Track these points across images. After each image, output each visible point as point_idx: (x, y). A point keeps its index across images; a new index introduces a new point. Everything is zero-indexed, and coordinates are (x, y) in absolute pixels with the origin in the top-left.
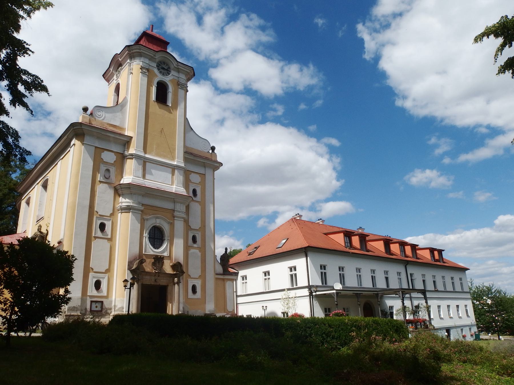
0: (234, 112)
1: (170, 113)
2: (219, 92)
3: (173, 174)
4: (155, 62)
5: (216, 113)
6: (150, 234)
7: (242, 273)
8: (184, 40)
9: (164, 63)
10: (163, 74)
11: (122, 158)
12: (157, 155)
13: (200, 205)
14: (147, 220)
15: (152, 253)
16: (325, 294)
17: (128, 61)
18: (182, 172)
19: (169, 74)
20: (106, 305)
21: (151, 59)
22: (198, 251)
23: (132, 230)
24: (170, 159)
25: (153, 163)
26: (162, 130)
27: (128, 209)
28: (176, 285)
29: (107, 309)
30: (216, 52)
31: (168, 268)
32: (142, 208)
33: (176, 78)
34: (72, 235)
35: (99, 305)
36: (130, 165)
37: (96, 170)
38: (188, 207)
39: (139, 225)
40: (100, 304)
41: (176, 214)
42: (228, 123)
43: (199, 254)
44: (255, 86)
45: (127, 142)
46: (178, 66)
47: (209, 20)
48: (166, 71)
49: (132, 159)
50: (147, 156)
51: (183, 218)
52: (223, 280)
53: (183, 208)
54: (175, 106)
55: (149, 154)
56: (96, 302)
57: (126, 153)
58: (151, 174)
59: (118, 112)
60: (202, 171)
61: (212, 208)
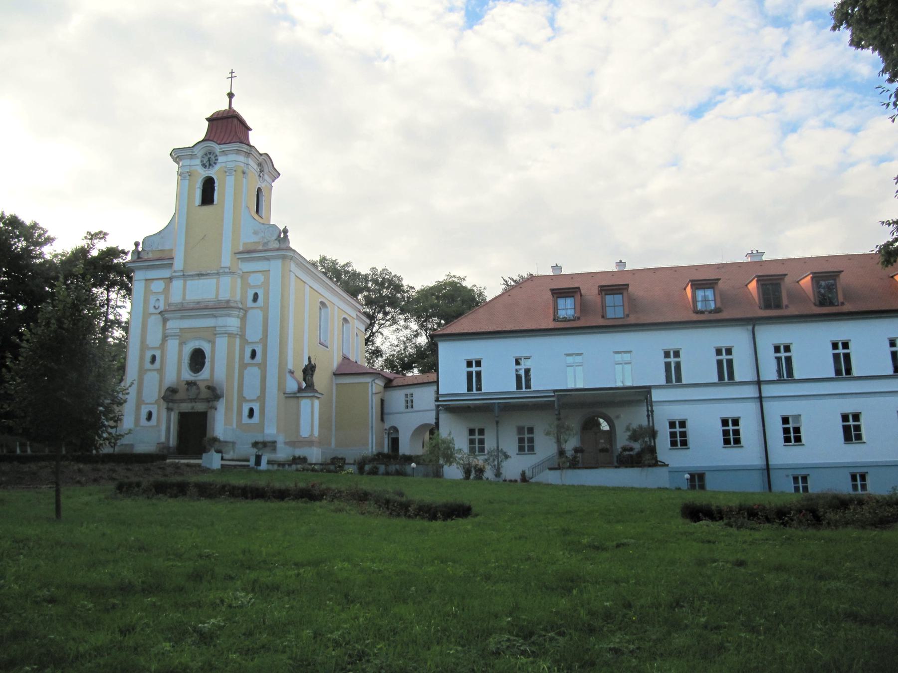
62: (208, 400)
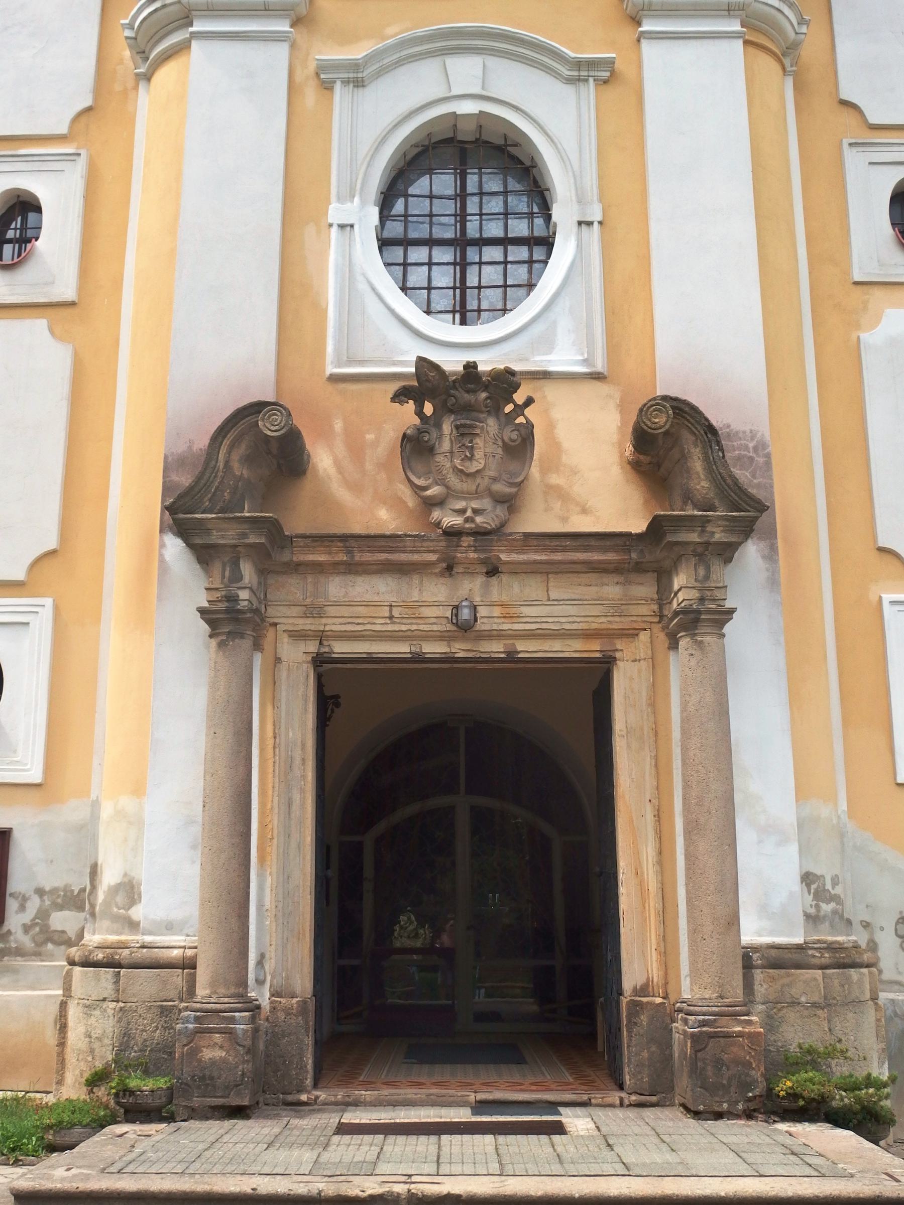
31: (587, 477)
62: (644, 555)
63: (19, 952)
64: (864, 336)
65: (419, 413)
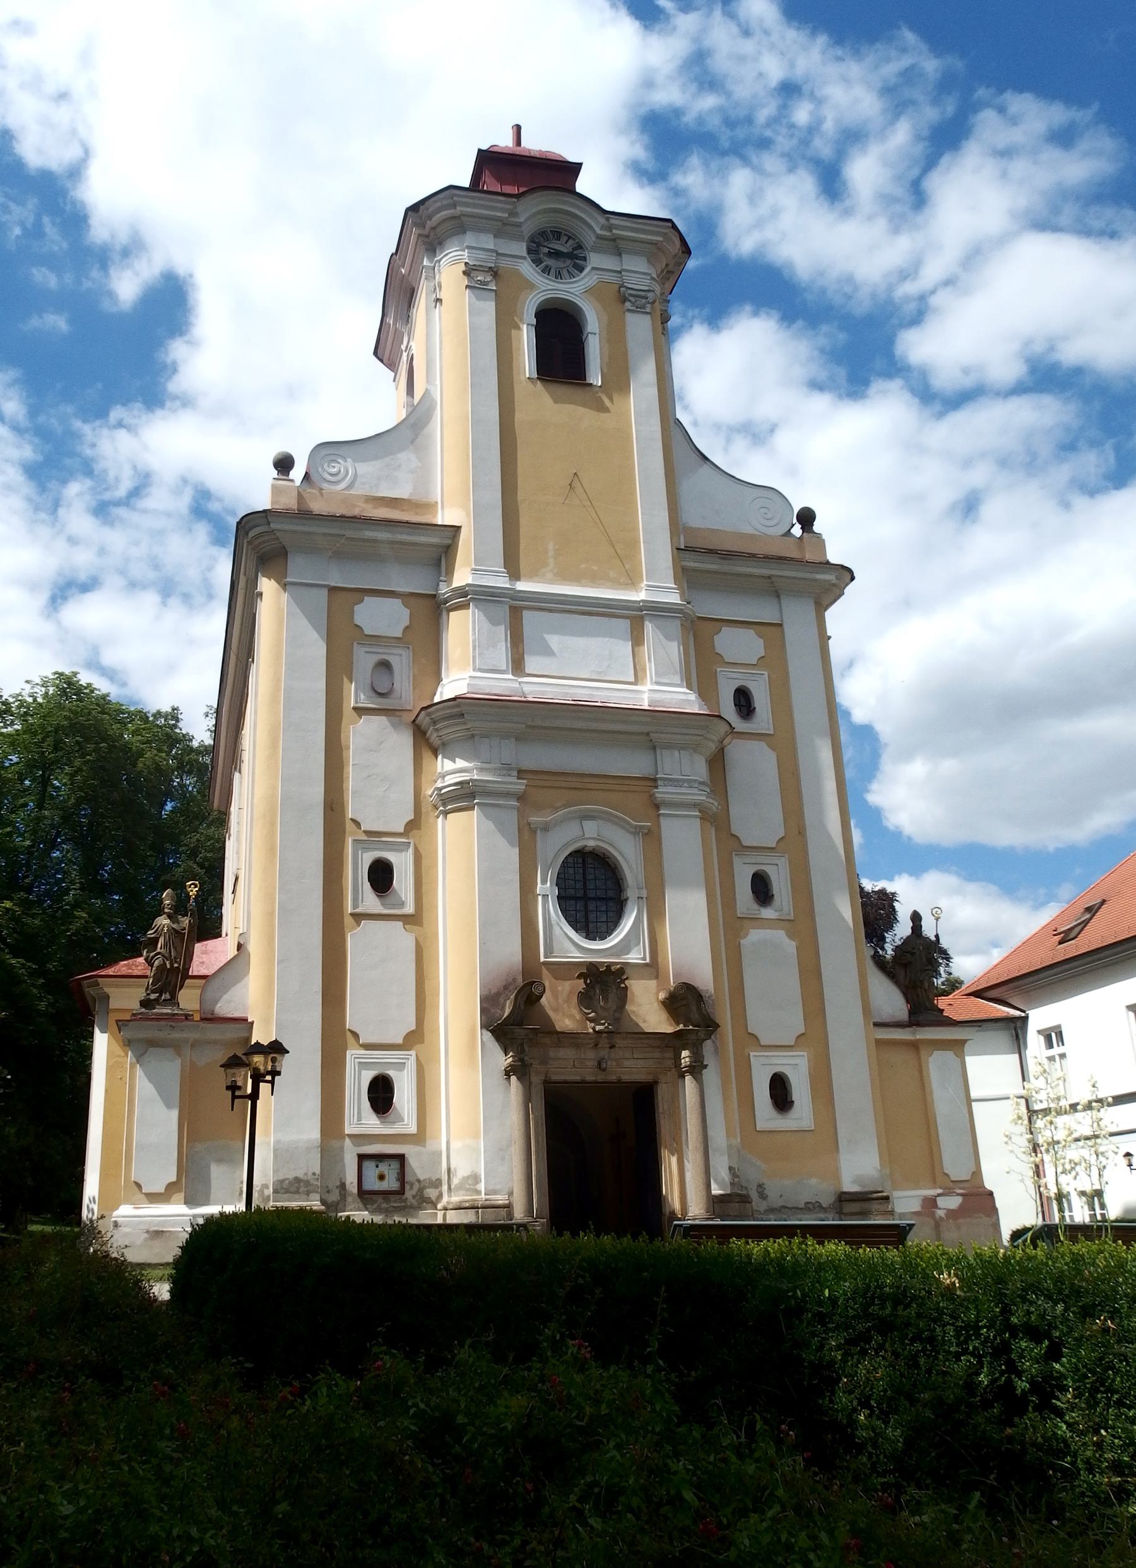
0: (1004, 462)
1: (602, 408)
2: (938, 407)
3: (637, 639)
4: (517, 237)
5: (941, 485)
6: (561, 881)
7: (1040, 1017)
8: (790, 265)
9: (557, 235)
10: (559, 275)
11: (432, 611)
12: (564, 576)
13: (773, 748)
14: (546, 828)
15: (576, 956)
16: (736, 1065)
17: (426, 262)
18: (675, 626)
19: (581, 269)
20: (417, 1166)
21: (503, 229)
22: (781, 934)
23: (488, 877)
24: (617, 584)
25: (550, 611)
26: (574, 482)
27: (464, 796)
28: (688, 1079)
29: (422, 1186)
30: (908, 273)
31: (648, 1011)
32: (520, 786)
33: (609, 277)
34: (272, 914)
35: (390, 1170)
36: (462, 630)
37: (338, 669)
38: (718, 763)
39: (513, 854)
40: (395, 1165)
41: (663, 792)
42: (990, 510)
43: (790, 946)
44: (1071, 353)
45: (443, 547)
46: (610, 228)
47: (865, 172)
48: (568, 262)
49: (464, 606)
50: (521, 586)
51: (695, 805)
52: (915, 1046)
53: (699, 769)
54: (619, 378)
55: (533, 575)
56: (379, 1158)
57: (444, 589)
58: (548, 652)
59: (401, 450)
60: (764, 611)
61: (826, 755)
63: (412, 1207)
64: (742, 942)
65: (585, 982)
